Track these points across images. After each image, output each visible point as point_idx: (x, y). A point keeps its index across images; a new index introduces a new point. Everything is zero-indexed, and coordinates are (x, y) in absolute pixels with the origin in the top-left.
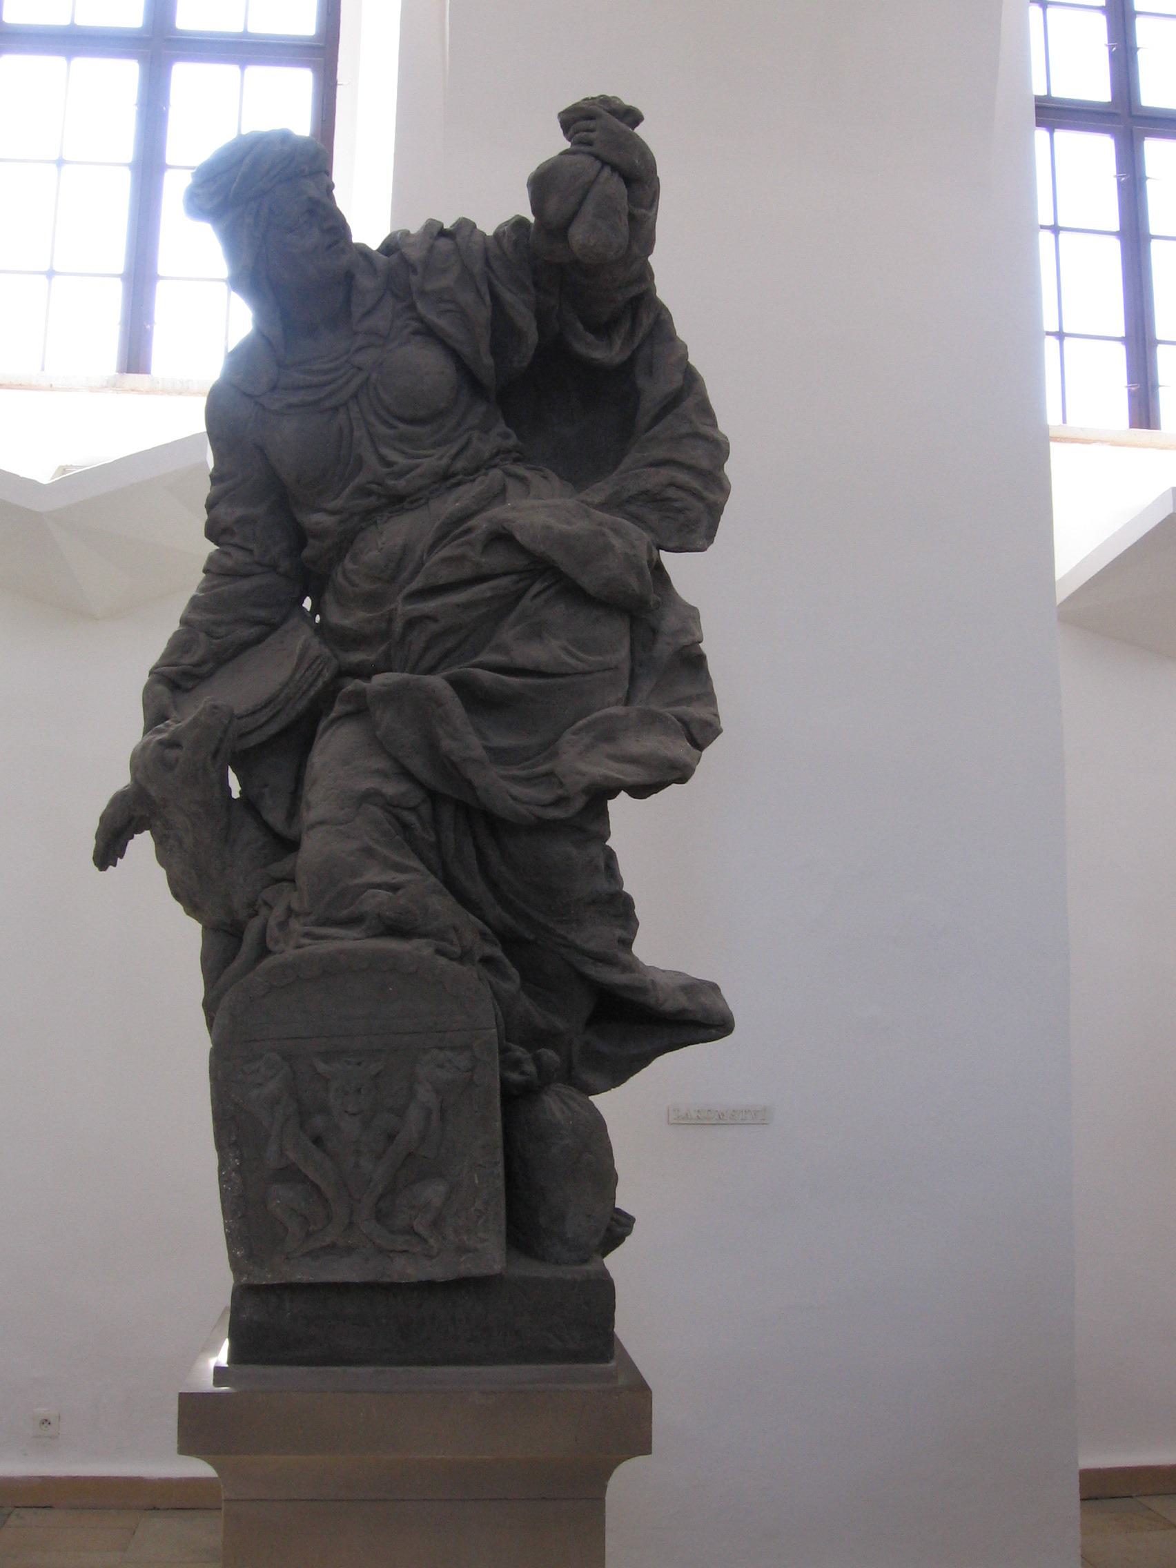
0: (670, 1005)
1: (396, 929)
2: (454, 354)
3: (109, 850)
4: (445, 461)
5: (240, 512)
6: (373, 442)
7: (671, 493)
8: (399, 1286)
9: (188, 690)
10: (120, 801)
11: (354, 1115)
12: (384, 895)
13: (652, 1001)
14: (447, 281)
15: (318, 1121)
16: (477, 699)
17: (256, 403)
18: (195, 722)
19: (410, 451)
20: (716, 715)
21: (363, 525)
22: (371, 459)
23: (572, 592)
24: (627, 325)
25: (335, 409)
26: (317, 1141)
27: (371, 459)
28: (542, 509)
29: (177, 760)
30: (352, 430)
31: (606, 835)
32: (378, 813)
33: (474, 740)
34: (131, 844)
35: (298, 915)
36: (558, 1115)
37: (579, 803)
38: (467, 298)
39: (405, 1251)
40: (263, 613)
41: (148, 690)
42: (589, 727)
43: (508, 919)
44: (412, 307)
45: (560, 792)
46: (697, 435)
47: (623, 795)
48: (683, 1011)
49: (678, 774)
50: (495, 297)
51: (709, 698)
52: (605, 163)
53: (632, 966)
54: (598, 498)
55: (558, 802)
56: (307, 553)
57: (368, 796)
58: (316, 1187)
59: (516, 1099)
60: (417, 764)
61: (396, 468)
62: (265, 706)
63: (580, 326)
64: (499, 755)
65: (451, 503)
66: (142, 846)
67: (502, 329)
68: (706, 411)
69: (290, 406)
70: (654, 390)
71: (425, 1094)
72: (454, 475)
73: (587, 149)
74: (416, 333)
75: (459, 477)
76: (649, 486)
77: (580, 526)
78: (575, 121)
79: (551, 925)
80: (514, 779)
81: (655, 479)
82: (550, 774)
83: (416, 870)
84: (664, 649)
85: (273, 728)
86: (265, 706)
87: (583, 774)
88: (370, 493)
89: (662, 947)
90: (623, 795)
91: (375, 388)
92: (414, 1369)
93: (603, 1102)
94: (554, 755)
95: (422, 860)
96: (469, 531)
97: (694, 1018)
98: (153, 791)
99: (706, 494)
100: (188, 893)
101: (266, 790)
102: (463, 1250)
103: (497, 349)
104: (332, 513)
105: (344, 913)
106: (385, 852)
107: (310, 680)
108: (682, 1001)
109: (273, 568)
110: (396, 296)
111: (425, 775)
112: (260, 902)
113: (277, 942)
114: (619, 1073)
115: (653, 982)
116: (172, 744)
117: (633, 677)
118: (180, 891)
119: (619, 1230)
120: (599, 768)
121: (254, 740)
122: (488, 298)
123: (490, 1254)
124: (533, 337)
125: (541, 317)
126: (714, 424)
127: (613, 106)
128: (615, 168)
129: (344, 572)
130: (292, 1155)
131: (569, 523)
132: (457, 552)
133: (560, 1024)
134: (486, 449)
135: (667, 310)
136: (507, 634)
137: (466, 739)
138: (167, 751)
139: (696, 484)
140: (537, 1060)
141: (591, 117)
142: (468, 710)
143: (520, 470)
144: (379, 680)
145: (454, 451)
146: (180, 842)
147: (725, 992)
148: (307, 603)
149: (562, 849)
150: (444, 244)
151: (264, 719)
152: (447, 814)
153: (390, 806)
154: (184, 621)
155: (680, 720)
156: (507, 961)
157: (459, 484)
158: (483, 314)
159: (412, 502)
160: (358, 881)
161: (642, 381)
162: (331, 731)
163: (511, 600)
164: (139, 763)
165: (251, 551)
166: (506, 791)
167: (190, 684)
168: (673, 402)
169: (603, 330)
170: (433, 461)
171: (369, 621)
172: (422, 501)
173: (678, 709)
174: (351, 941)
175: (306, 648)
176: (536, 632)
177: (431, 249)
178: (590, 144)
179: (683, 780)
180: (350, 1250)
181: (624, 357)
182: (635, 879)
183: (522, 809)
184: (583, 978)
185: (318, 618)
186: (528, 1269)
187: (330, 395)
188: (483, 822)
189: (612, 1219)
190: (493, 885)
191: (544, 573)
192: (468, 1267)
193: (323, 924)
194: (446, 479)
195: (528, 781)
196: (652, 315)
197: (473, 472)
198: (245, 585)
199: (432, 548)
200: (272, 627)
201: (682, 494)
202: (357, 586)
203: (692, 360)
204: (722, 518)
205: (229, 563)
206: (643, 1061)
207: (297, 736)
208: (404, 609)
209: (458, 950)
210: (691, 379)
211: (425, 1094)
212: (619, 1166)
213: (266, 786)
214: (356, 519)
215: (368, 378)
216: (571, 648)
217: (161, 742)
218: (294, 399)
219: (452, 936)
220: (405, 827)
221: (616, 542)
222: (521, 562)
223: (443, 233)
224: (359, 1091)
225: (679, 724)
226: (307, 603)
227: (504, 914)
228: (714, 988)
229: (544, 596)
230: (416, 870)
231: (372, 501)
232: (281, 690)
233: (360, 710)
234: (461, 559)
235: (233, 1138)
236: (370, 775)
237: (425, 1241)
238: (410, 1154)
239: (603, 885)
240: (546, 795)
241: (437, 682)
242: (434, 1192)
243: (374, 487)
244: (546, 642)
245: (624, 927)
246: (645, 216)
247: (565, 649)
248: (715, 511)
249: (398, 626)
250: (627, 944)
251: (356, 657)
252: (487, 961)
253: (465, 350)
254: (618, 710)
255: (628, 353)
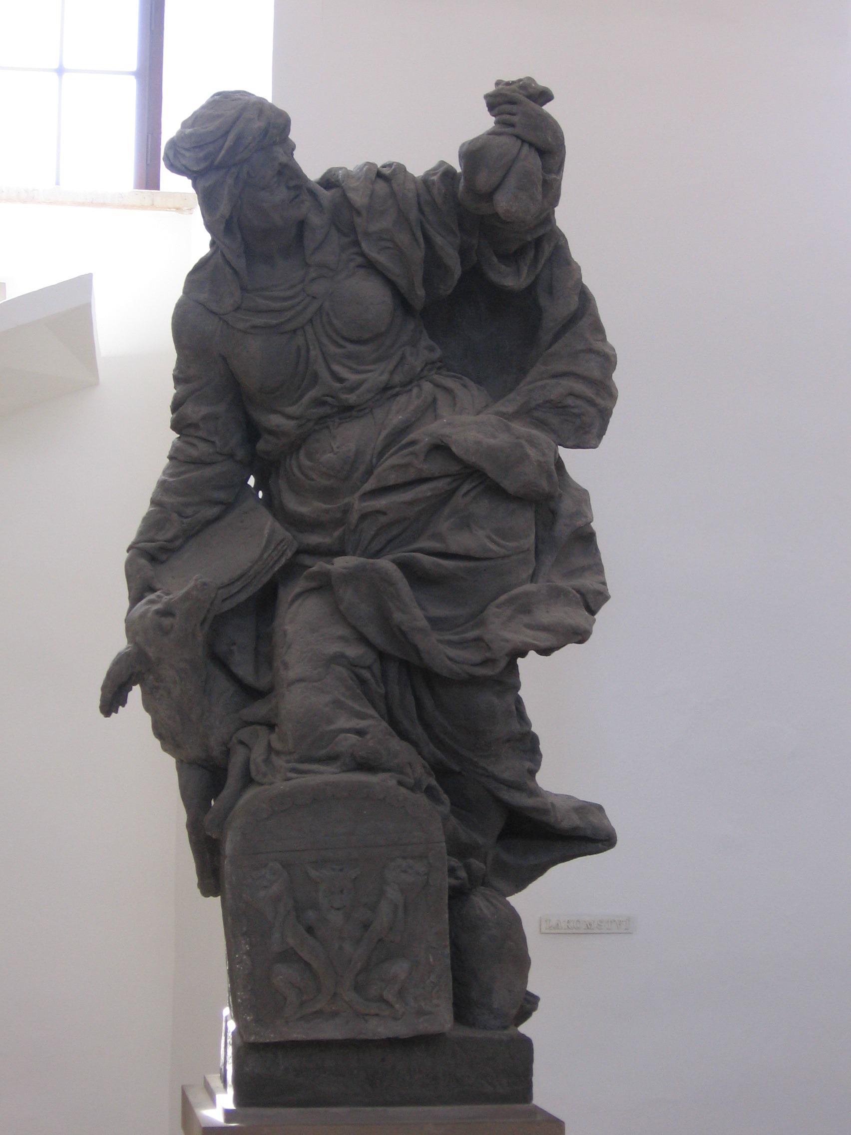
0: (566, 824)
1: (365, 765)
2: (391, 284)
3: (112, 701)
4: (385, 377)
5: (204, 410)
6: (325, 359)
7: (570, 401)
8: (372, 1041)
9: (162, 562)
10: (121, 661)
11: (338, 909)
12: (353, 738)
13: (552, 820)
14: (385, 223)
15: (311, 914)
16: (417, 576)
17: (220, 319)
18: (187, 597)
19: (355, 366)
20: (604, 584)
21: (316, 428)
22: (324, 374)
23: (495, 491)
24: (531, 254)
25: (294, 331)
26: (310, 930)
27: (324, 374)
28: (471, 423)
29: (172, 626)
30: (308, 351)
31: (517, 687)
32: (344, 672)
33: (418, 612)
34: (130, 694)
35: (278, 753)
36: (486, 911)
37: (503, 664)
38: (403, 238)
39: (377, 1015)
40: (221, 495)
41: (129, 564)
42: (511, 601)
43: (440, 755)
44: (357, 243)
45: (488, 655)
46: (591, 351)
47: (532, 654)
48: (576, 829)
49: (580, 638)
50: (427, 239)
51: (597, 568)
52: (523, 141)
53: (535, 792)
54: (510, 409)
55: (485, 663)
56: (261, 446)
57: (337, 659)
58: (307, 964)
59: (458, 895)
60: (372, 632)
61: (347, 384)
62: (238, 580)
63: (495, 259)
64: (435, 622)
65: (396, 414)
66: (136, 694)
67: (433, 262)
68: (598, 328)
69: (254, 327)
70: (556, 311)
71: (393, 893)
72: (392, 388)
73: (509, 130)
74: (360, 266)
75: (397, 389)
76: (552, 397)
77: (502, 440)
78: (500, 104)
79: (475, 760)
80: (450, 643)
81: (557, 389)
82: (479, 640)
83: (372, 717)
84: (562, 529)
85: (243, 597)
86: (238, 580)
87: (507, 641)
88: (324, 403)
89: (561, 776)
90: (532, 654)
91: (328, 314)
92: (380, 1109)
93: (515, 900)
94: (482, 623)
95: (375, 707)
96: (413, 443)
97: (582, 835)
98: (151, 652)
99: (599, 401)
100: (168, 735)
101: (234, 648)
102: (421, 1013)
103: (427, 281)
104: (289, 417)
105: (323, 752)
106: (350, 703)
107: (276, 558)
108: (575, 821)
109: (231, 456)
110: (339, 230)
111: (379, 640)
112: (234, 740)
113: (265, 775)
114: (522, 881)
115: (552, 804)
116: (166, 613)
117: (537, 553)
118: (159, 731)
119: (528, 1006)
120: (518, 635)
121: (227, 606)
122: (421, 240)
123: (442, 1019)
124: (458, 272)
125: (463, 252)
126: (604, 339)
127: (531, 90)
128: (531, 145)
129: (300, 467)
130: (291, 941)
131: (495, 437)
132: (403, 461)
133: (480, 840)
134: (416, 362)
135: (564, 236)
136: (444, 525)
137: (413, 612)
138: (163, 619)
139: (589, 392)
140: (468, 868)
141: (512, 102)
142: (411, 587)
143: (449, 383)
144: (341, 563)
145: (391, 367)
146: (169, 693)
147: (609, 813)
148: (252, 481)
149: (487, 699)
150: (381, 187)
151: (236, 590)
152: (393, 671)
153: (353, 666)
154: (153, 502)
155: (578, 591)
156: (440, 789)
157: (397, 395)
158: (418, 254)
159: (360, 411)
160: (332, 727)
161: (544, 301)
162: (299, 601)
163: (446, 497)
164: (132, 628)
165: (213, 443)
166: (443, 653)
167: (164, 557)
168: (573, 319)
169: (513, 258)
170: (376, 376)
171: (327, 511)
172: (367, 411)
173: (578, 582)
174: (328, 775)
175: (273, 532)
176: (466, 523)
177: (372, 195)
178: (512, 125)
179: (581, 642)
180: (335, 1014)
181: (529, 281)
182: (539, 721)
183: (456, 667)
184: (498, 801)
185: (260, 494)
186: (464, 1032)
187: (289, 320)
188: (419, 674)
189: (525, 999)
190: (427, 726)
191: (474, 477)
192: (424, 1026)
193: (303, 762)
194: (387, 391)
195: (462, 644)
196: (553, 244)
197: (407, 384)
198: (208, 472)
199: (381, 454)
200: (228, 507)
201: (579, 402)
202: (312, 480)
203: (586, 280)
204: (611, 420)
205: (194, 453)
206: (539, 870)
207: (264, 603)
208: (359, 506)
209: (412, 781)
210: (585, 298)
211: (393, 893)
212: (531, 953)
213: (234, 644)
214: (311, 424)
215: (321, 305)
216: (494, 537)
217: (158, 613)
218: (259, 321)
219: (409, 770)
220: (362, 682)
221: (531, 452)
222: (454, 468)
223: (379, 175)
224: (342, 891)
225: (578, 595)
226: (252, 481)
227: (436, 750)
228: (600, 808)
229: (472, 494)
230: (372, 717)
231: (326, 410)
232: (251, 567)
233: (324, 585)
234: (407, 466)
235: (245, 929)
236: (334, 642)
237: (391, 1006)
238: (380, 940)
239: (516, 727)
240: (477, 657)
241: (385, 563)
242: (400, 968)
243: (329, 399)
244: (477, 531)
245: (531, 761)
246: (555, 179)
247: (489, 537)
248: (605, 415)
249: (354, 517)
250: (532, 773)
251: (314, 539)
252: (429, 791)
253: (402, 283)
254: (529, 587)
255: (533, 278)
